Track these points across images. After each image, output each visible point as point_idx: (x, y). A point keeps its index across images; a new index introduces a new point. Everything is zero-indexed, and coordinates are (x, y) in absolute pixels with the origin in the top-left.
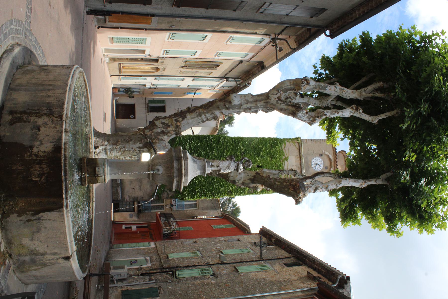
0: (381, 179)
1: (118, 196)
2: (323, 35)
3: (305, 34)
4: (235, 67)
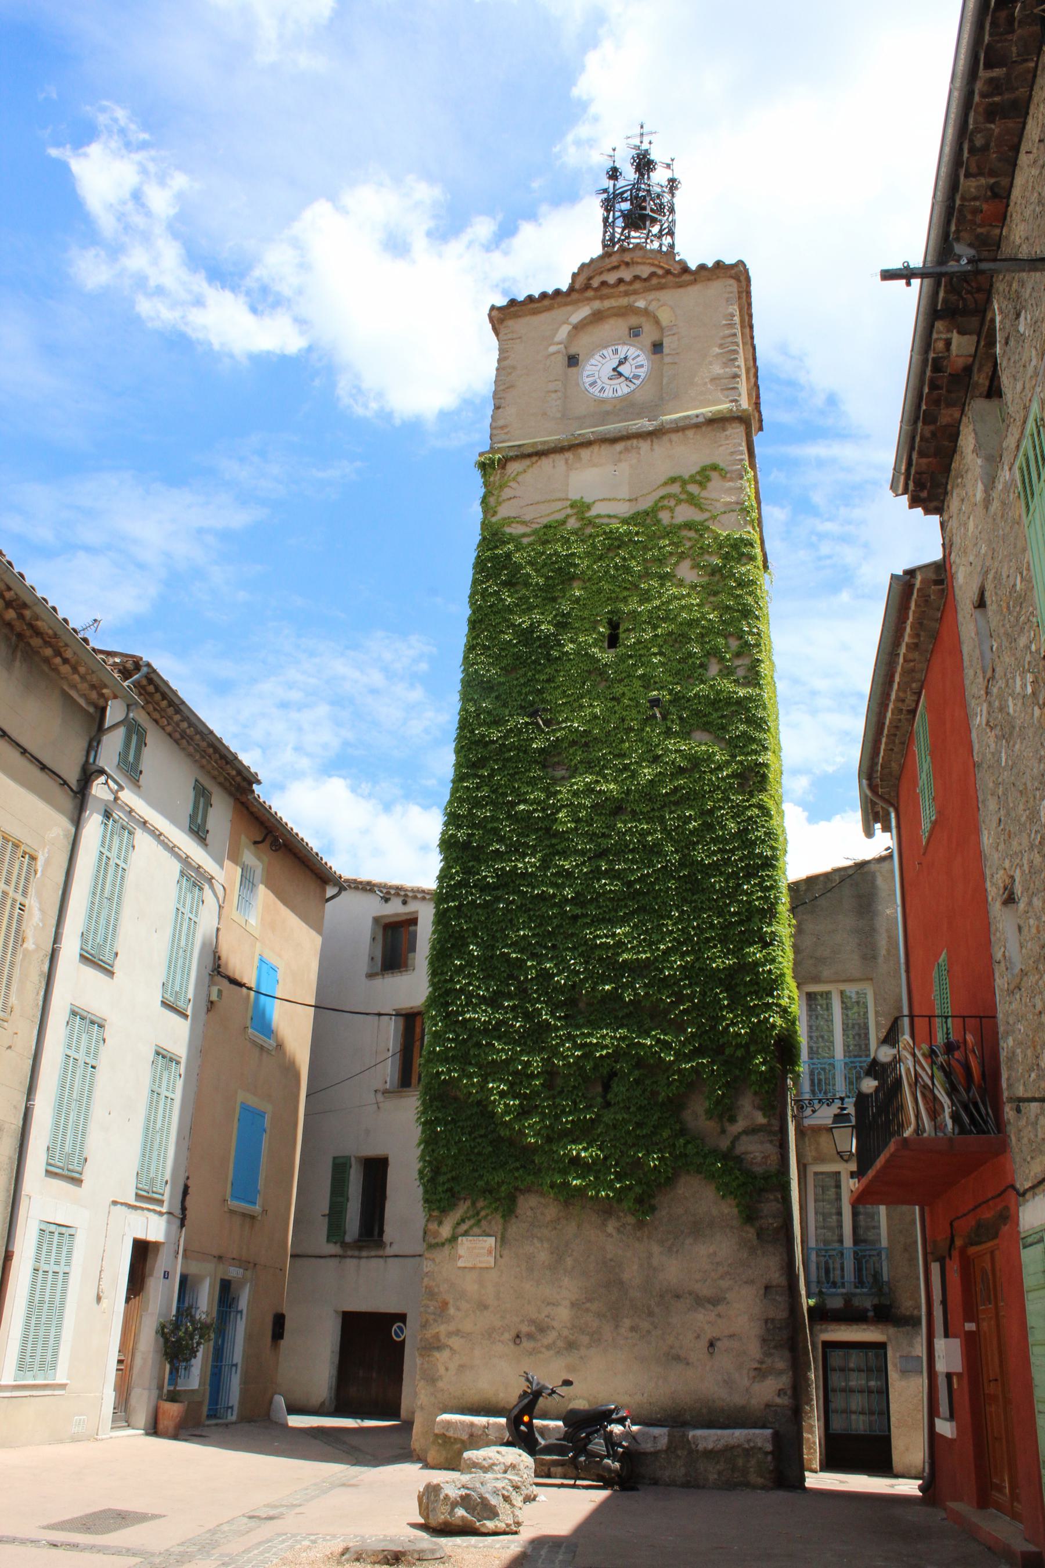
1: (748, 1452)
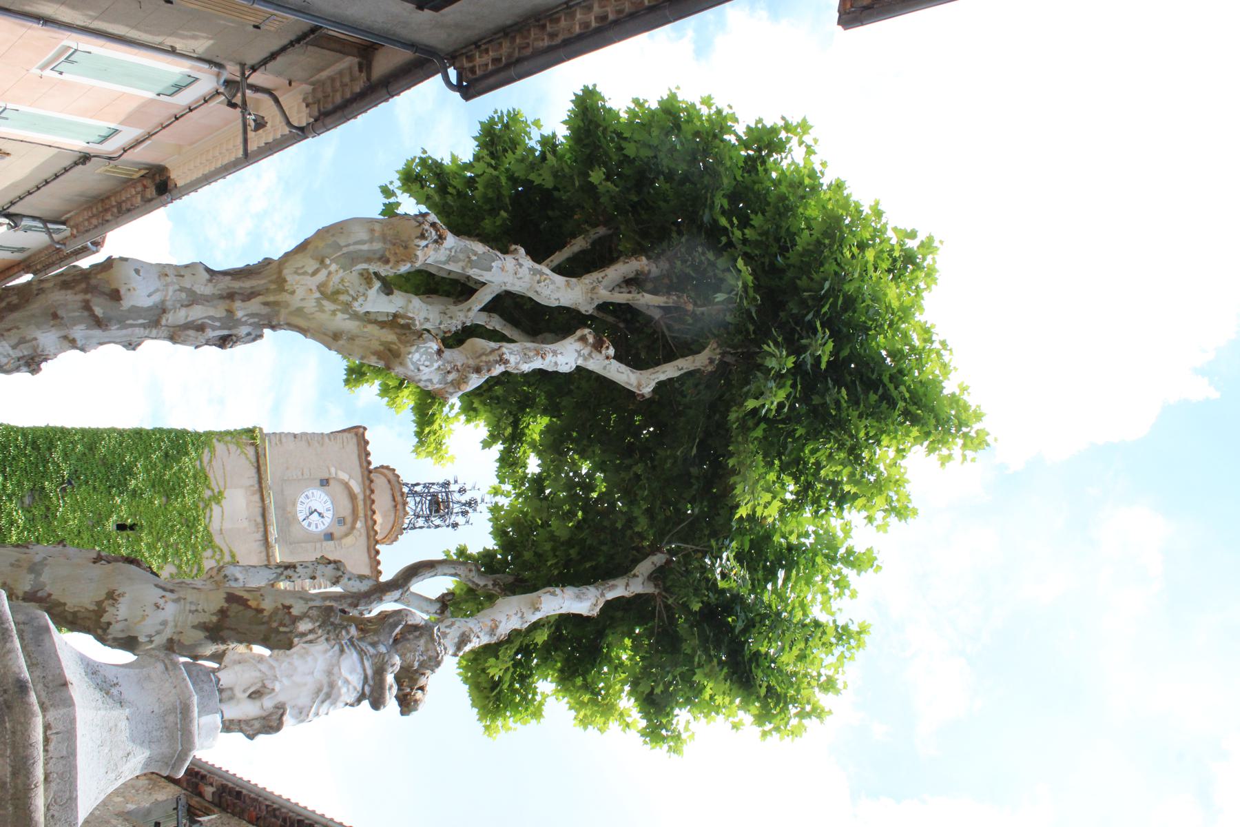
0: (640, 579)
2: (438, 78)
3: (347, 79)
4: (57, 176)
